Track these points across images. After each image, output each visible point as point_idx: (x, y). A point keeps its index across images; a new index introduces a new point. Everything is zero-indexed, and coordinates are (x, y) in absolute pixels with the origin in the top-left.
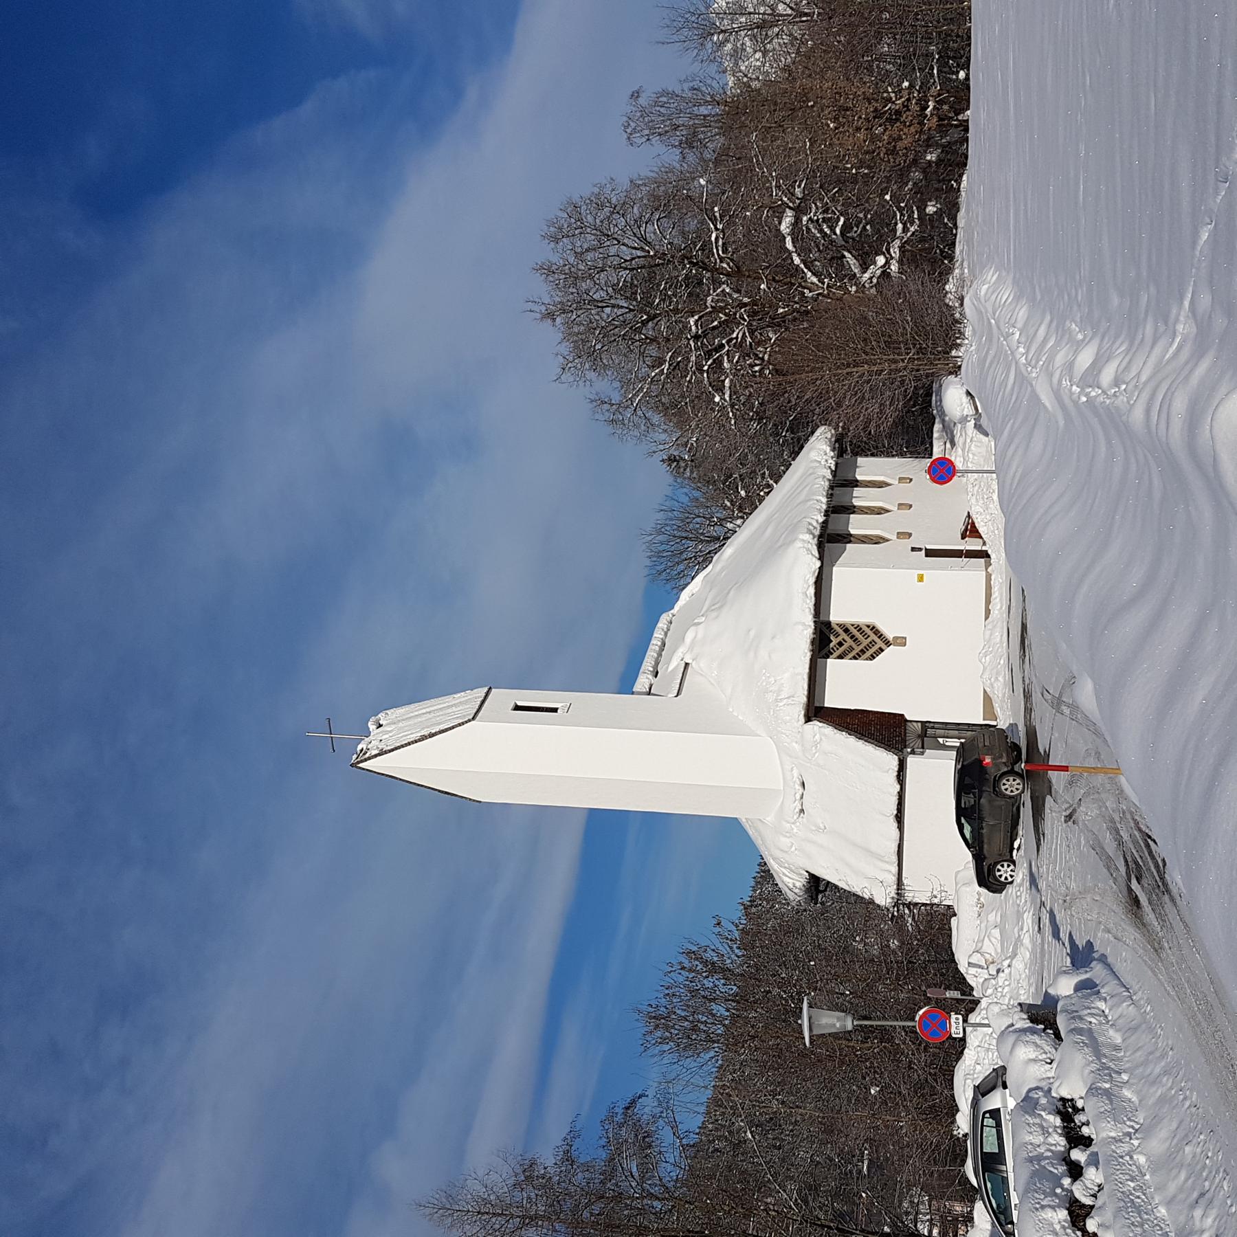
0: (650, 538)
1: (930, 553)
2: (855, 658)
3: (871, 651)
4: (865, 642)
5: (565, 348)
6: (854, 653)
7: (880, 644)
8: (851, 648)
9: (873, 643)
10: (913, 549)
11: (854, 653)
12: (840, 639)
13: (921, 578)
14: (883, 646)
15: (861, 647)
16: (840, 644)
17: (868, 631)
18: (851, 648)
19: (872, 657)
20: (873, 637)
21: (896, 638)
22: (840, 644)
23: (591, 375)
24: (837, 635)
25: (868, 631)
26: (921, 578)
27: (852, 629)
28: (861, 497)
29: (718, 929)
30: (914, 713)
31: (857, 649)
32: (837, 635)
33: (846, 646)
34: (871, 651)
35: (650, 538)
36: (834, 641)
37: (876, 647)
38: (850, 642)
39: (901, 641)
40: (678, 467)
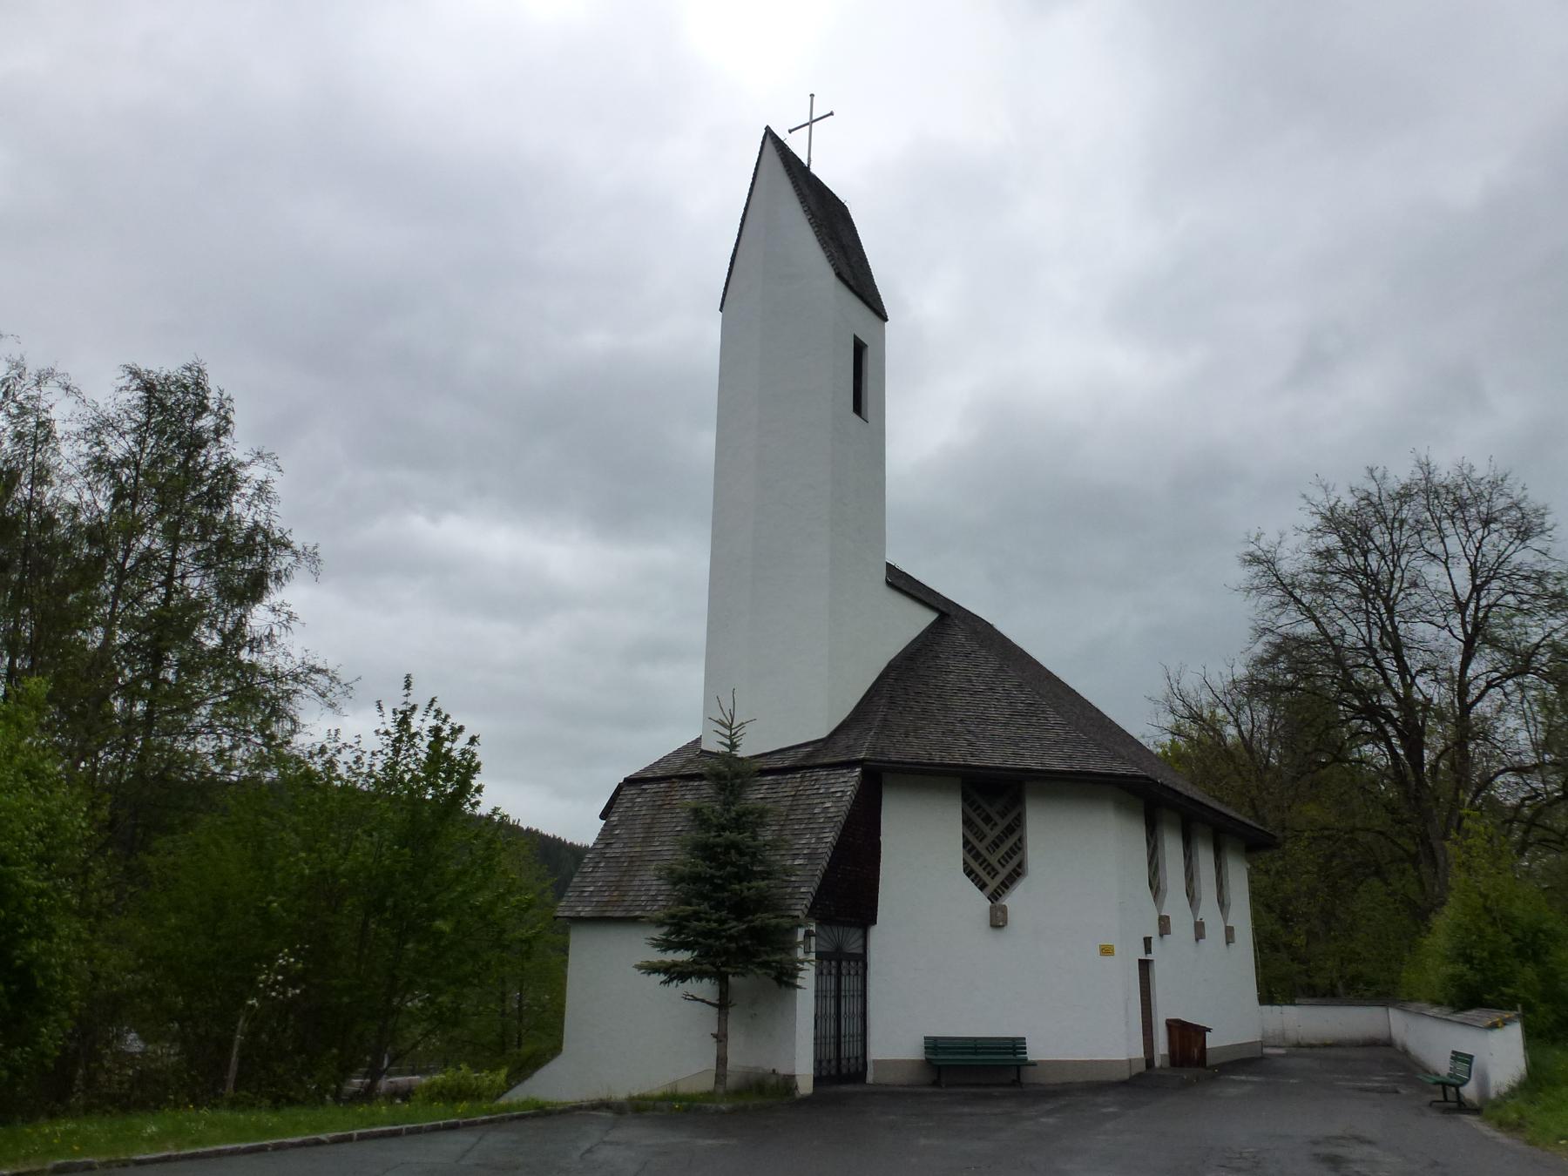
1: (1145, 966)
2: (966, 843)
4: (993, 860)
7: (993, 884)
13: (1106, 951)
15: (984, 852)
19: (969, 872)
20: (1003, 873)
26: (1106, 951)
37: (987, 879)
38: (992, 834)
39: (998, 920)
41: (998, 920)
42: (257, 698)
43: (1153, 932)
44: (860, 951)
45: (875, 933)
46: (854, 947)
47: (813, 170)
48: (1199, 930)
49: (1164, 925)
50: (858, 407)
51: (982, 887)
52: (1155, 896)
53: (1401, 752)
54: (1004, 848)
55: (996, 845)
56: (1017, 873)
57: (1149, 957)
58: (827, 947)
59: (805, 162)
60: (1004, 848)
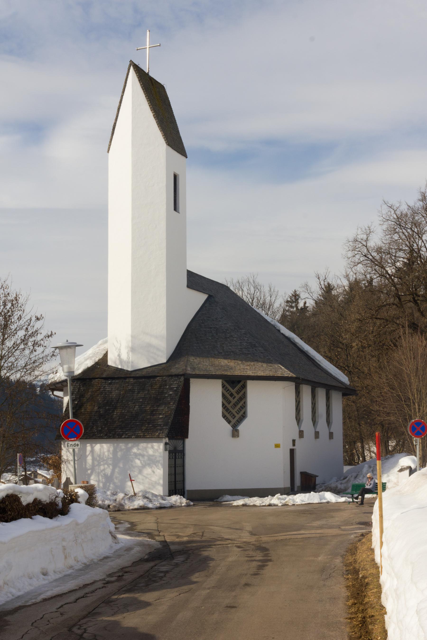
0: (252, 281)
1: (292, 452)
2: (223, 405)
3: (228, 415)
4: (234, 412)
5: (404, 209)
6: (226, 404)
7: (233, 421)
8: (229, 402)
9: (234, 417)
10: (294, 441)
11: (226, 404)
12: (235, 394)
13: (277, 446)
14: (232, 423)
15: (231, 409)
16: (231, 395)
17: (241, 413)
18: (229, 402)
19: (224, 416)
20: (238, 416)
21: (237, 431)
22: (231, 395)
23: (385, 227)
24: (238, 393)
25: (241, 413)
26: (277, 446)
27: (242, 403)
28: (321, 394)
29: (34, 319)
30: (190, 444)
31: (229, 406)
32: (238, 393)
33: (231, 399)
34: (228, 415)
35: (252, 281)
36: (233, 391)
37: (231, 419)
38: (233, 401)
39: (235, 433)
40: (292, 302)
41: (235, 433)
42: (386, 454)
43: (296, 436)
44: (182, 449)
45: (187, 441)
46: (180, 448)
47: (151, 74)
48: (317, 435)
49: (301, 434)
50: (176, 208)
51: (229, 422)
52: (314, 425)
53: (84, 463)
54: (239, 406)
55: (235, 405)
56: (244, 416)
57: (294, 448)
58: (172, 449)
59: (147, 72)
60: (239, 406)
